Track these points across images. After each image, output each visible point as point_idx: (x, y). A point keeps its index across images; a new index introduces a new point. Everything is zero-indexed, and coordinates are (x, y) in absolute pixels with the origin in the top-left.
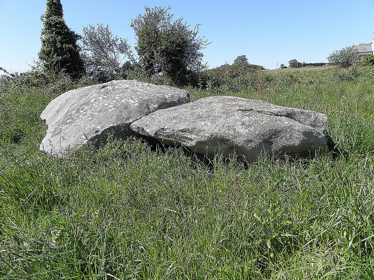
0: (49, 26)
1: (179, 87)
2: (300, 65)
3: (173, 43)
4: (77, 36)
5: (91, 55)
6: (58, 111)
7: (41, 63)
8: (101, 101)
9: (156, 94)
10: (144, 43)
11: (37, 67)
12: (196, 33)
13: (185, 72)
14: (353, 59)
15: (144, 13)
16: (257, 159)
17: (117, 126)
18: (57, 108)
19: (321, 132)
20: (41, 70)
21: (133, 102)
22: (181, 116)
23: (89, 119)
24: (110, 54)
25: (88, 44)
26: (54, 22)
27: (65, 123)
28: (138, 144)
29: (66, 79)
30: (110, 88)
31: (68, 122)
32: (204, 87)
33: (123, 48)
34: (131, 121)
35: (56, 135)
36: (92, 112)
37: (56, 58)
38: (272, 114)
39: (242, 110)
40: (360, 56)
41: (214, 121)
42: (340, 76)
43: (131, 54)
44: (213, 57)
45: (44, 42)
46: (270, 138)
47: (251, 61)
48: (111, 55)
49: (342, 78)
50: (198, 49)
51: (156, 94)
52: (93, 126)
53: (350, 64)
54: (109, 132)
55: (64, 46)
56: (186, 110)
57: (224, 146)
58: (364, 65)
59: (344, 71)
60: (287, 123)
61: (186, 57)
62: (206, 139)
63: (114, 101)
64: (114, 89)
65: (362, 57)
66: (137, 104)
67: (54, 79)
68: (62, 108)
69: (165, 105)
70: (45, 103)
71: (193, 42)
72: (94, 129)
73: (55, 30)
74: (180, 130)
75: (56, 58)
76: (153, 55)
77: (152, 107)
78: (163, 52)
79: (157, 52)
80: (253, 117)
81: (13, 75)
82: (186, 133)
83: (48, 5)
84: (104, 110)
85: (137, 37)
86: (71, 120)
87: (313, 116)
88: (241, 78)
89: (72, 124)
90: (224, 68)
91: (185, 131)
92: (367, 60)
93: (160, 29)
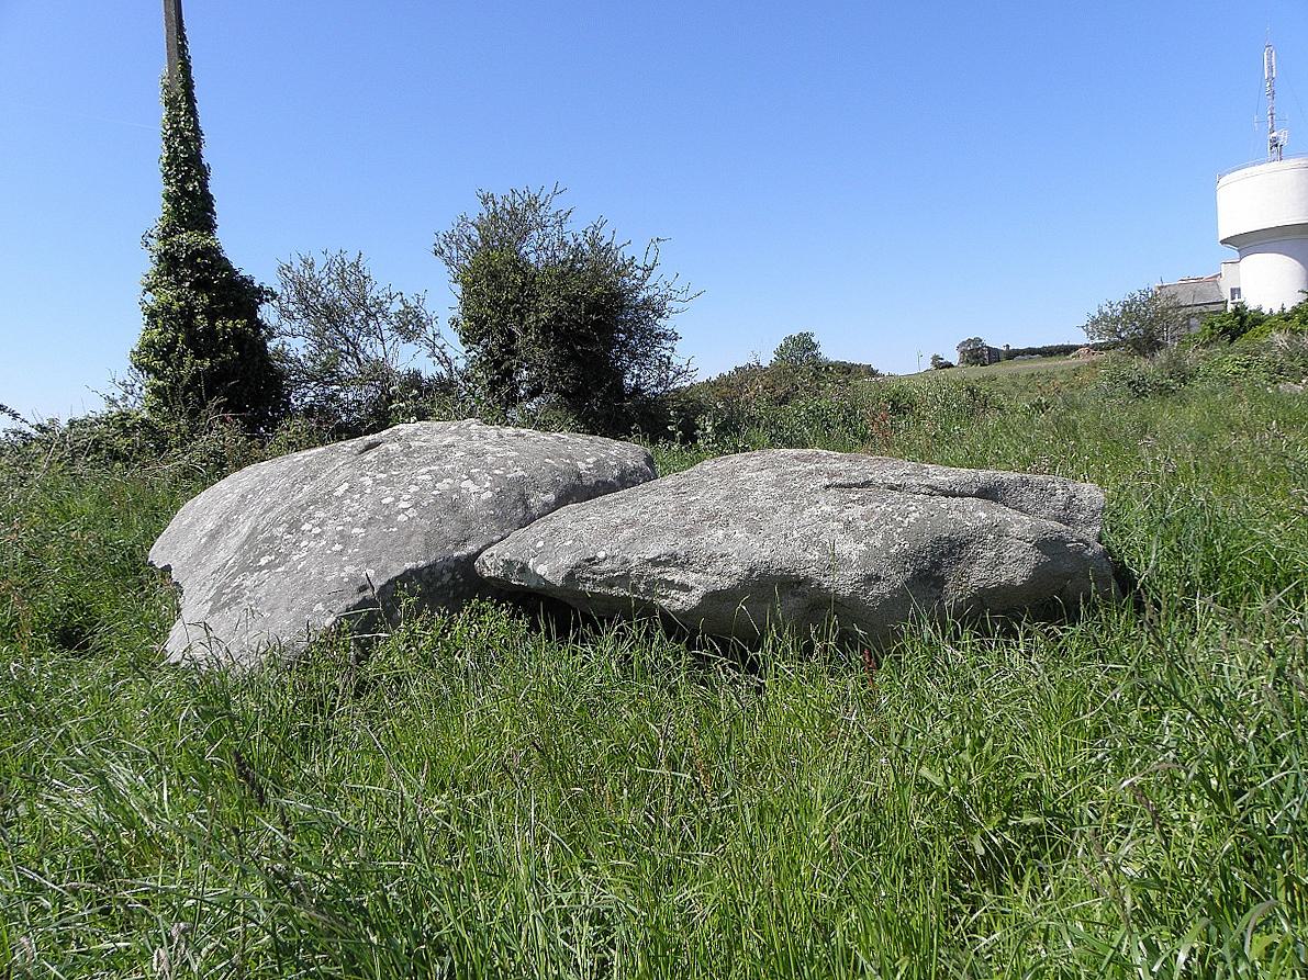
0: (170, 262)
1: (616, 438)
2: (994, 356)
3: (575, 300)
4: (259, 291)
5: (305, 352)
6: (214, 536)
7: (138, 385)
8: (368, 491)
9: (547, 460)
10: (481, 304)
11: (125, 399)
12: (650, 264)
13: (618, 390)
14: (1168, 327)
15: (476, 210)
16: (902, 633)
17: (429, 566)
18: (210, 526)
19: (1092, 540)
20: (139, 405)
21: (474, 488)
22: (646, 516)
23: (333, 549)
24: (368, 346)
25: (295, 315)
26: (187, 250)
27: (245, 568)
28: (497, 621)
29: (223, 433)
30: (394, 447)
31: (263, 562)
32: (689, 437)
33: (411, 325)
34: (471, 548)
35: (224, 606)
36: (341, 528)
37: (190, 366)
38: (934, 490)
39: (841, 486)
40: (1189, 317)
41: (753, 528)
42: (1133, 382)
43: (439, 342)
44: (706, 343)
45: (152, 315)
46: (936, 565)
47: (830, 352)
48: (372, 349)
49: (1138, 388)
50: (660, 316)
51: (547, 460)
52: (350, 569)
53: (1159, 344)
54: (403, 588)
55: (219, 324)
56: (657, 499)
57: (792, 602)
58: (1206, 345)
59: (1142, 366)
60: (983, 515)
61: (624, 344)
62: (734, 581)
63: (413, 489)
64: (408, 452)
65: (1193, 321)
66: (489, 494)
67: (183, 435)
68: (226, 523)
69: (578, 491)
70: (158, 518)
71: (643, 295)
72: (353, 579)
73: (191, 276)
74: (649, 560)
75: (190, 366)
76: (513, 342)
77: (538, 499)
78: (545, 330)
79: (525, 330)
80: (877, 504)
81: (41, 428)
82: (667, 569)
83: (168, 198)
84: (381, 517)
85: (458, 288)
86: (273, 557)
87: (1061, 491)
88: (798, 399)
89: (279, 570)
90: (746, 374)
91: (666, 563)
92: (1212, 328)
93: (532, 258)
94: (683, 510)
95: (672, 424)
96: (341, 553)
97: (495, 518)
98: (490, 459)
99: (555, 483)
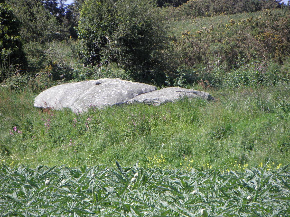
21: (124, 92)
41: (167, 96)
66: (127, 93)
78: (120, 39)
94: (159, 94)
95: (167, 80)
96: (104, 101)
97: (128, 97)
98: (126, 87)
99: (138, 92)
